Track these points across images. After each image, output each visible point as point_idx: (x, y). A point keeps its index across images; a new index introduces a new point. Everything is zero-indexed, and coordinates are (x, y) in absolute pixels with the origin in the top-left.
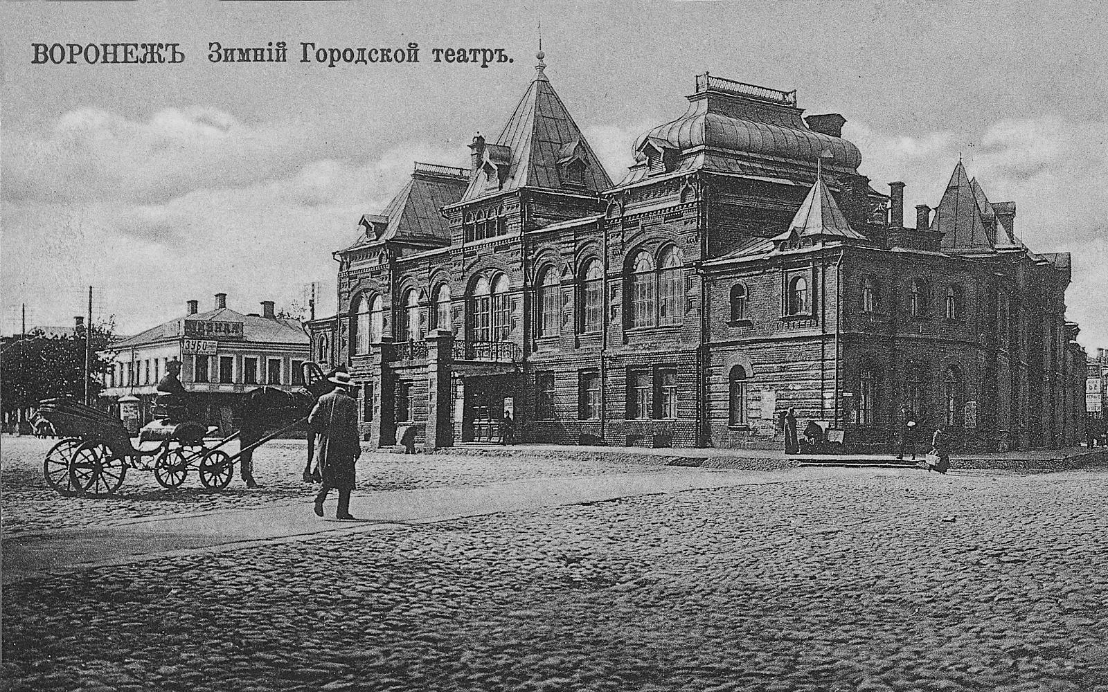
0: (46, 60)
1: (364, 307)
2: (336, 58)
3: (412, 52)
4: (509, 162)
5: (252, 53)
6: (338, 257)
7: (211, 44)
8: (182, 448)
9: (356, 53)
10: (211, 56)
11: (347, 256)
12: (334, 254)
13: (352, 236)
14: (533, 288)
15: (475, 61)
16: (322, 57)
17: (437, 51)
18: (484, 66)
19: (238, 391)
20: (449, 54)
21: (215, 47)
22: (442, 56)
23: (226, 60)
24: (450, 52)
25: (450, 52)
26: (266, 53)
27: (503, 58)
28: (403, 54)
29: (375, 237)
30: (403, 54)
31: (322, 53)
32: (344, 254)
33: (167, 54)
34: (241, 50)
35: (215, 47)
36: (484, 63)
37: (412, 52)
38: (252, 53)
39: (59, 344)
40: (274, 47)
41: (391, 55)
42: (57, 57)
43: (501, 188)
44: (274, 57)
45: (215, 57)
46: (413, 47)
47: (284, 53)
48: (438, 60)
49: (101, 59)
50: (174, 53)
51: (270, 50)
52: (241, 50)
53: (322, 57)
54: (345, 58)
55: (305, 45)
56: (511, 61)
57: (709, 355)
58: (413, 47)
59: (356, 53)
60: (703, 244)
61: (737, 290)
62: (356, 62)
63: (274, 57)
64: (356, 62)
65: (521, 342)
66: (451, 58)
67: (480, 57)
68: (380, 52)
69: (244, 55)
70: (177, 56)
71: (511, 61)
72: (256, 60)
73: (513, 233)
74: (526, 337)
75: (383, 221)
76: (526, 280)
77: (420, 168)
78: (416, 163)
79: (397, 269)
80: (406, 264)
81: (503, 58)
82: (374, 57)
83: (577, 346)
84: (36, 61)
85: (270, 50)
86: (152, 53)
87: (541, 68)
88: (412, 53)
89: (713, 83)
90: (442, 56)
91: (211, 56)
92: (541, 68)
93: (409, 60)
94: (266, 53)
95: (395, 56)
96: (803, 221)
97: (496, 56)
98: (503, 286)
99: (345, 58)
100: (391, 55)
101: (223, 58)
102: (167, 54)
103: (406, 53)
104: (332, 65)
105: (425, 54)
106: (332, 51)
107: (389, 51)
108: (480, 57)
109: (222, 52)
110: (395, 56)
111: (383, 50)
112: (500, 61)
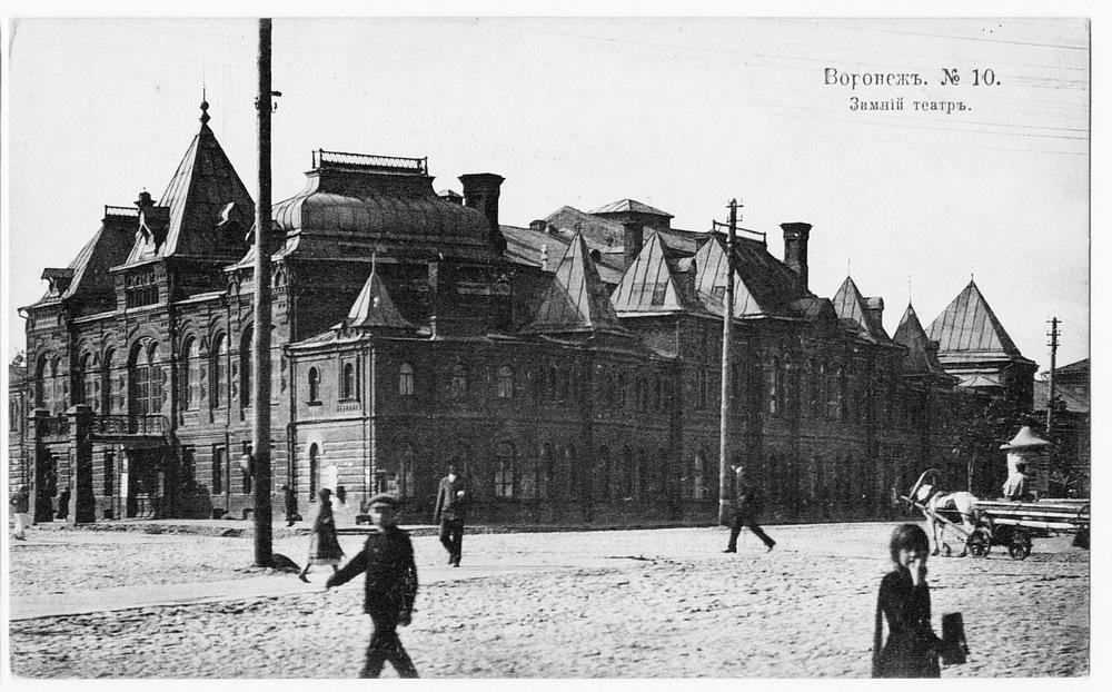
1: (48, 373)
6: (24, 313)
11: (34, 313)
12: (20, 310)
13: (38, 291)
14: (180, 359)
21: (855, 100)
22: (920, 106)
27: (962, 107)
29: (58, 294)
32: (30, 310)
35: (855, 100)
43: (156, 252)
57: (295, 431)
60: (292, 328)
61: (313, 372)
65: (169, 414)
69: (874, 106)
73: (162, 303)
74: (174, 410)
75: (67, 275)
76: (174, 352)
77: (112, 213)
78: (106, 207)
79: (74, 330)
81: (962, 107)
83: (212, 421)
87: (205, 118)
89: (326, 157)
90: (920, 106)
92: (205, 118)
96: (512, 250)
98: (157, 357)
108: (946, 106)
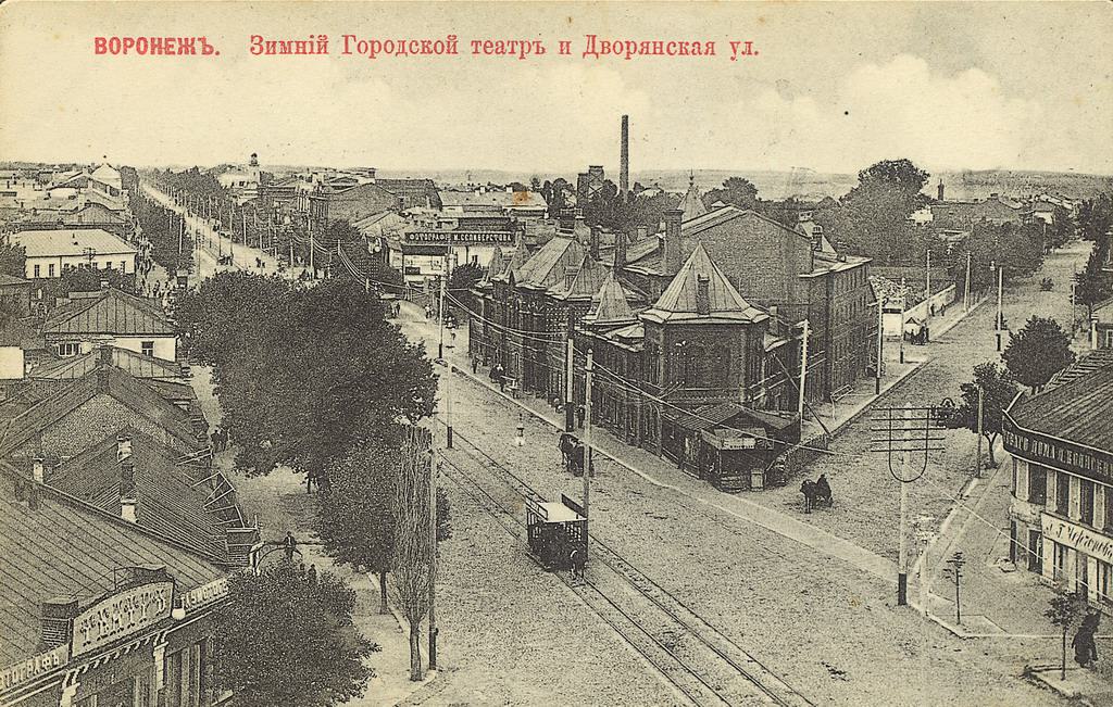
0: (609, 51)
2: (632, 51)
3: (451, 44)
5: (294, 46)
7: (253, 38)
9: (396, 45)
10: (253, 49)
15: (513, 52)
16: (363, 50)
17: (476, 43)
18: (522, 57)
20: (487, 45)
21: (257, 40)
22: (480, 49)
23: (268, 53)
24: (488, 44)
25: (488, 44)
26: (308, 46)
27: (208, 50)
28: (443, 46)
30: (443, 46)
31: (389, 49)
33: (198, 46)
34: (282, 43)
36: (522, 55)
37: (451, 44)
38: (294, 46)
40: (315, 40)
41: (690, 48)
42: (389, 48)
44: (316, 50)
45: (257, 49)
46: (452, 39)
47: (454, 45)
48: (476, 52)
49: (445, 51)
50: (538, 46)
51: (312, 43)
52: (282, 43)
53: (363, 50)
54: (385, 50)
55: (347, 37)
58: (452, 39)
59: (396, 45)
62: (397, 54)
63: (316, 50)
64: (397, 54)
66: (489, 50)
67: (518, 48)
68: (421, 44)
69: (286, 48)
70: (541, 51)
71: (218, 53)
72: (298, 52)
80: (756, 368)
81: (208, 50)
82: (414, 48)
85: (312, 43)
86: (187, 47)
88: (451, 46)
90: (480, 49)
91: (253, 49)
93: (268, 53)
94: (308, 46)
97: (534, 48)
99: (385, 50)
100: (431, 47)
101: (265, 51)
104: (372, 57)
105: (464, 46)
106: (373, 42)
107: (687, 44)
108: (518, 48)
109: (264, 44)
111: (681, 43)
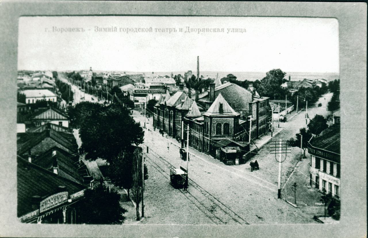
4: (187, 173)
8: (41, 197)
19: (143, 203)
21: (96, 28)
22: (158, 30)
39: (338, 98)
41: (217, 30)
48: (156, 31)
52: (104, 29)
56: (228, 33)
84: (223, 29)
90: (158, 30)
91: (95, 30)
95: (146, 30)
102: (81, 30)
103: (149, 29)
106: (62, 29)
107: (216, 29)
108: (168, 31)
110: (146, 30)
112: (174, 31)
